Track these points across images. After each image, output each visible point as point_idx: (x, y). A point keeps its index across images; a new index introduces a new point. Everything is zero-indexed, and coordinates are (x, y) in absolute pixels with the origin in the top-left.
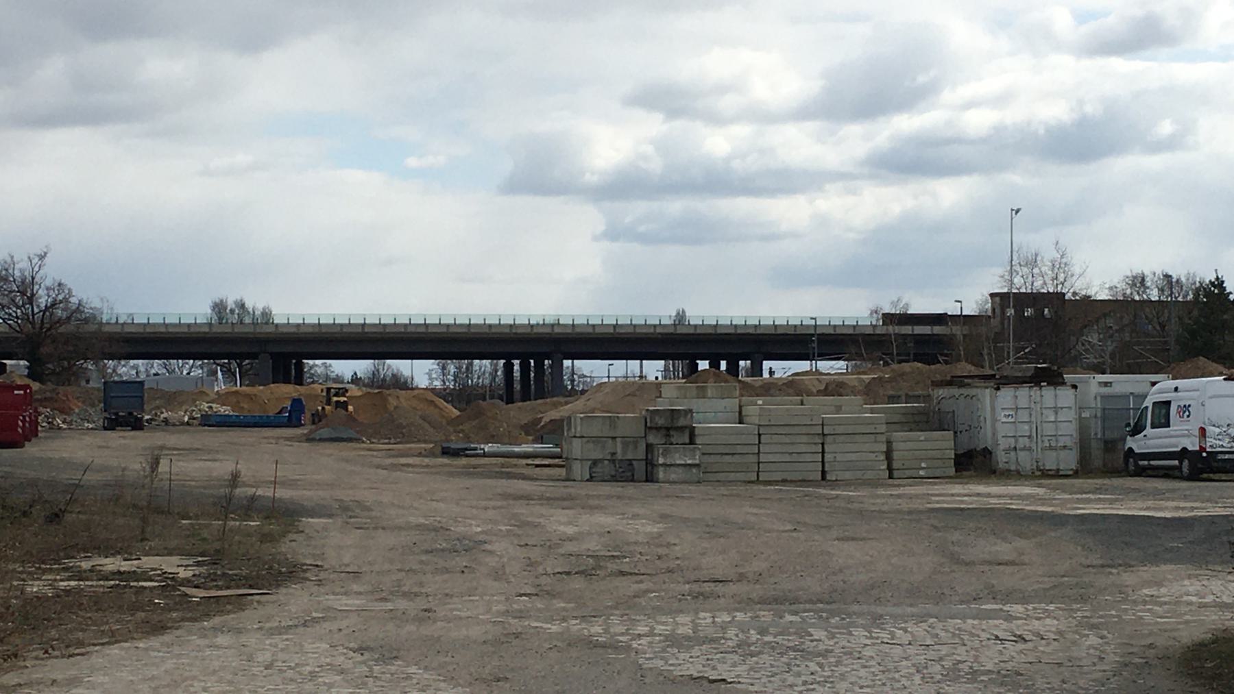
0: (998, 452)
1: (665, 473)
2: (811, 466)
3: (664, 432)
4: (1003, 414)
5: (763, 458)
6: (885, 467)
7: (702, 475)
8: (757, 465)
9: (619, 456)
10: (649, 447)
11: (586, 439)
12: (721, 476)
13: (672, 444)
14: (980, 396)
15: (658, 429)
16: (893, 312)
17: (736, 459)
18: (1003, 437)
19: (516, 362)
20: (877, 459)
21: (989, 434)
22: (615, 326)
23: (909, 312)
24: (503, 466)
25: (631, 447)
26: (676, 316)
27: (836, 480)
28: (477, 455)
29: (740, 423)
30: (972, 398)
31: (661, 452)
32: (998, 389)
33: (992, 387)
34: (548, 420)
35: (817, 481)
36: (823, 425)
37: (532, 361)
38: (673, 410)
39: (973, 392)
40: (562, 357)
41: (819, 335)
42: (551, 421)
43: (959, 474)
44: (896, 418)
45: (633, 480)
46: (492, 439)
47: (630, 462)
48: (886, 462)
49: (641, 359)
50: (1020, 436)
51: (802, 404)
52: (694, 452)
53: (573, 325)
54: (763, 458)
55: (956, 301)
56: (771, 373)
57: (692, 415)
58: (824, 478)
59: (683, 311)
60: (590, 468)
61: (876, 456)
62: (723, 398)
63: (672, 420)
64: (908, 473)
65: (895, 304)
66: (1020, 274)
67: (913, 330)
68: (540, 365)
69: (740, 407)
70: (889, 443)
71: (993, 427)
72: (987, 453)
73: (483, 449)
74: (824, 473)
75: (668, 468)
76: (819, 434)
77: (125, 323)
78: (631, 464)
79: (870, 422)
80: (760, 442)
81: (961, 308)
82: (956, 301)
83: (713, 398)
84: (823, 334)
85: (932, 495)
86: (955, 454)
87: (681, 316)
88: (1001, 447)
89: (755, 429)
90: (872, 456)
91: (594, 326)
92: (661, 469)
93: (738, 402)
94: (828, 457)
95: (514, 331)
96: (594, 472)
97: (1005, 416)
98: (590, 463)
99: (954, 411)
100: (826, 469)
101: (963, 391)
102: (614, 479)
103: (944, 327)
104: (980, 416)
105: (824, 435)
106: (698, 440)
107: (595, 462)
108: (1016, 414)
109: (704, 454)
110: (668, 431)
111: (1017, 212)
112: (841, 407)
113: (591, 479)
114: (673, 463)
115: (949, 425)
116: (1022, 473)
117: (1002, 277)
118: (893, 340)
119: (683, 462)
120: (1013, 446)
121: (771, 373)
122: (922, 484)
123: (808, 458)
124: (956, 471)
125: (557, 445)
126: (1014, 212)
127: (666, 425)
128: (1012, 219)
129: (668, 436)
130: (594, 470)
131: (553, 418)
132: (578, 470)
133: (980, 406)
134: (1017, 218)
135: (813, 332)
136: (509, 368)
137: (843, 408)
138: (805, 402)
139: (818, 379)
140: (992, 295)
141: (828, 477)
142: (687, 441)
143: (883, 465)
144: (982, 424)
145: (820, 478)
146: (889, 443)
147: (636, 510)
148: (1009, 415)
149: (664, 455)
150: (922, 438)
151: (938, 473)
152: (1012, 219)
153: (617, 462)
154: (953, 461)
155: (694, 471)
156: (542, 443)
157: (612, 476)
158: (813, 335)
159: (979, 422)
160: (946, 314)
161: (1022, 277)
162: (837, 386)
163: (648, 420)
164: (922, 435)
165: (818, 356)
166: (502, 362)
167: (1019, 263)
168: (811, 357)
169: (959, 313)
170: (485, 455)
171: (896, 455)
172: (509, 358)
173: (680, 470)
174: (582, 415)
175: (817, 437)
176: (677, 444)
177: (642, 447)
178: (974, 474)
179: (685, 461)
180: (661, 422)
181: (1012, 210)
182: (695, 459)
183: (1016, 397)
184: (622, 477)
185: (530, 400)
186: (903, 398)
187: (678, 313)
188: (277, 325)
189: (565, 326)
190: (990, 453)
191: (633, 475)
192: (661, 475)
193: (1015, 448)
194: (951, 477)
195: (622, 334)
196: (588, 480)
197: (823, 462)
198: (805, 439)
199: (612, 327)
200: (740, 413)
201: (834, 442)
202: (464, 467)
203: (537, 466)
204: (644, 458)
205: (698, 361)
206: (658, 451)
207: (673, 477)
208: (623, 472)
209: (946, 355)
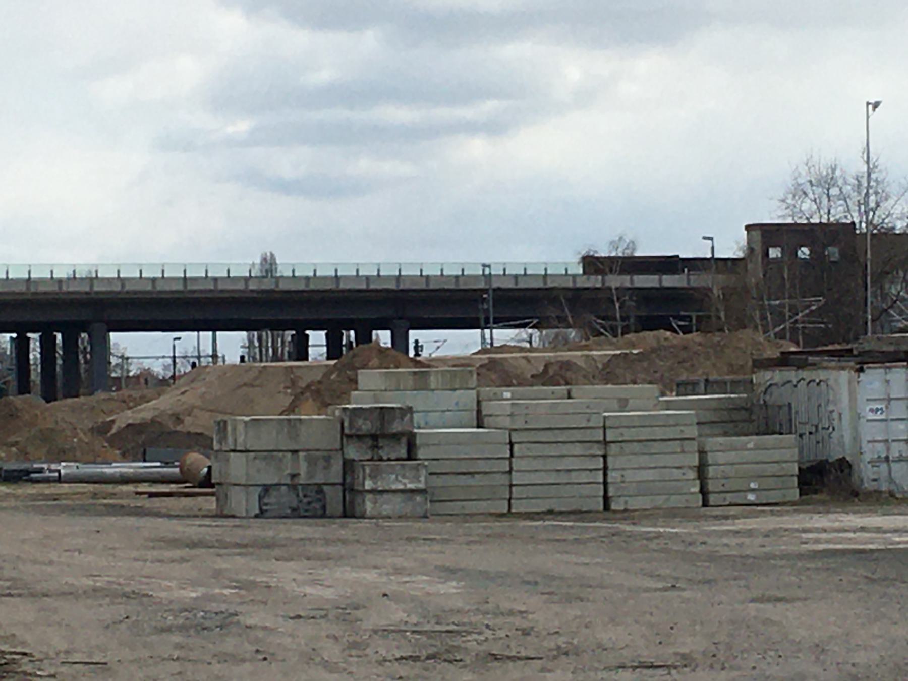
0: (862, 466)
1: (375, 503)
2: (586, 490)
3: (370, 442)
4: (868, 408)
5: (516, 479)
6: (696, 489)
7: (429, 504)
8: (508, 488)
9: (302, 480)
10: (347, 466)
11: (252, 454)
12: (455, 507)
13: (381, 459)
14: (831, 383)
15: (360, 437)
16: (613, 254)
17: (477, 481)
18: (869, 442)
19: (34, 337)
20: (685, 477)
21: (847, 439)
22: (399, 278)
23: (637, 254)
24: (95, 496)
25: (321, 463)
26: (261, 264)
27: (626, 510)
28: (47, 480)
29: (479, 427)
30: (818, 384)
31: (368, 471)
32: (861, 370)
33: (852, 368)
34: (123, 425)
35: (597, 512)
36: (604, 428)
37: (59, 336)
38: (382, 408)
39: (822, 375)
40: (408, 324)
41: (494, 290)
42: (129, 425)
43: (804, 497)
44: (709, 416)
45: (323, 516)
46: (61, 455)
47: (319, 489)
48: (698, 482)
49: (214, 330)
50: (894, 441)
51: (569, 397)
52: (418, 470)
53: (185, 279)
54: (516, 479)
55: (705, 238)
56: (417, 347)
57: (412, 419)
58: (607, 507)
59: (272, 255)
60: (260, 498)
61: (684, 474)
62: (455, 390)
63: (382, 425)
64: (730, 498)
65: (614, 244)
66: (811, 195)
67: (660, 281)
68: (70, 344)
69: (479, 402)
70: (702, 453)
71: (855, 429)
72: (844, 465)
73: (59, 471)
74: (606, 499)
75: (378, 497)
76: (598, 442)
77: (282, 277)
78: (320, 491)
79: (677, 422)
80: (512, 455)
81: (713, 248)
82: (705, 238)
83: (437, 389)
84: (499, 289)
85: (805, 531)
86: (800, 469)
87: (269, 263)
88: (867, 457)
89: (505, 433)
90: (677, 473)
91: (215, 280)
92: (369, 497)
93: (475, 397)
94: (612, 476)
95: (33, 290)
96: (266, 505)
97: (871, 410)
98: (260, 489)
99: (790, 404)
100: (610, 494)
101: (806, 374)
102: (296, 513)
103: (677, 277)
104: (832, 412)
105: (606, 443)
106: (421, 454)
107: (267, 489)
108: (887, 407)
109: (431, 474)
110: (375, 439)
111: (876, 105)
112: (627, 400)
113: (261, 514)
114: (387, 488)
115: (781, 425)
116: (898, 496)
117: (783, 201)
118: (615, 298)
119: (401, 487)
120: (883, 455)
121: (417, 347)
122: (757, 515)
123: (584, 477)
124: (801, 495)
125: (167, 463)
126: (870, 107)
127: (373, 432)
128: (868, 117)
129: (375, 447)
130: (266, 501)
131: (130, 421)
132: (241, 502)
133: (831, 398)
134: (875, 116)
135: (482, 285)
136: (21, 345)
137: (631, 401)
138: (573, 394)
139: (525, 358)
140: (748, 228)
141: (613, 507)
142: (403, 453)
143: (694, 486)
144: (836, 423)
145: (601, 508)
146: (702, 453)
147: (399, 561)
148: (877, 410)
149: (373, 477)
150: (751, 446)
151: (774, 497)
152: (868, 117)
153: (300, 488)
154: (796, 479)
155: (418, 499)
156: (145, 461)
157: (294, 510)
158: (485, 291)
159: (830, 420)
160: (678, 256)
161: (815, 201)
162: (561, 368)
163: (346, 424)
164: (751, 441)
165: (494, 323)
166: (289, 334)
167: (810, 182)
168: (482, 323)
169: (709, 256)
170: (59, 480)
171: (711, 471)
172: (21, 330)
173: (398, 498)
174: (247, 419)
175: (596, 446)
176: (389, 460)
177: (337, 466)
178: (828, 498)
179: (405, 484)
180: (365, 426)
181: (868, 104)
182: (420, 482)
183: (888, 382)
184: (306, 511)
185: (56, 400)
186: (702, 386)
187: (264, 260)
188: (278, 279)
189: (325, 278)
190: (850, 466)
191: (324, 508)
192: (369, 506)
193: (887, 458)
194: (793, 504)
195: (194, 291)
196: (257, 516)
197: (605, 483)
198: (578, 449)
199: (243, 282)
200: (479, 411)
201: (622, 453)
202: (34, 498)
203: (152, 495)
204: (340, 480)
205: (307, 332)
206: (364, 470)
207: (387, 509)
208: (309, 503)
209: (682, 318)
